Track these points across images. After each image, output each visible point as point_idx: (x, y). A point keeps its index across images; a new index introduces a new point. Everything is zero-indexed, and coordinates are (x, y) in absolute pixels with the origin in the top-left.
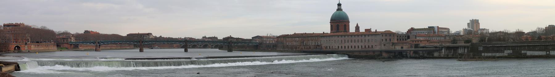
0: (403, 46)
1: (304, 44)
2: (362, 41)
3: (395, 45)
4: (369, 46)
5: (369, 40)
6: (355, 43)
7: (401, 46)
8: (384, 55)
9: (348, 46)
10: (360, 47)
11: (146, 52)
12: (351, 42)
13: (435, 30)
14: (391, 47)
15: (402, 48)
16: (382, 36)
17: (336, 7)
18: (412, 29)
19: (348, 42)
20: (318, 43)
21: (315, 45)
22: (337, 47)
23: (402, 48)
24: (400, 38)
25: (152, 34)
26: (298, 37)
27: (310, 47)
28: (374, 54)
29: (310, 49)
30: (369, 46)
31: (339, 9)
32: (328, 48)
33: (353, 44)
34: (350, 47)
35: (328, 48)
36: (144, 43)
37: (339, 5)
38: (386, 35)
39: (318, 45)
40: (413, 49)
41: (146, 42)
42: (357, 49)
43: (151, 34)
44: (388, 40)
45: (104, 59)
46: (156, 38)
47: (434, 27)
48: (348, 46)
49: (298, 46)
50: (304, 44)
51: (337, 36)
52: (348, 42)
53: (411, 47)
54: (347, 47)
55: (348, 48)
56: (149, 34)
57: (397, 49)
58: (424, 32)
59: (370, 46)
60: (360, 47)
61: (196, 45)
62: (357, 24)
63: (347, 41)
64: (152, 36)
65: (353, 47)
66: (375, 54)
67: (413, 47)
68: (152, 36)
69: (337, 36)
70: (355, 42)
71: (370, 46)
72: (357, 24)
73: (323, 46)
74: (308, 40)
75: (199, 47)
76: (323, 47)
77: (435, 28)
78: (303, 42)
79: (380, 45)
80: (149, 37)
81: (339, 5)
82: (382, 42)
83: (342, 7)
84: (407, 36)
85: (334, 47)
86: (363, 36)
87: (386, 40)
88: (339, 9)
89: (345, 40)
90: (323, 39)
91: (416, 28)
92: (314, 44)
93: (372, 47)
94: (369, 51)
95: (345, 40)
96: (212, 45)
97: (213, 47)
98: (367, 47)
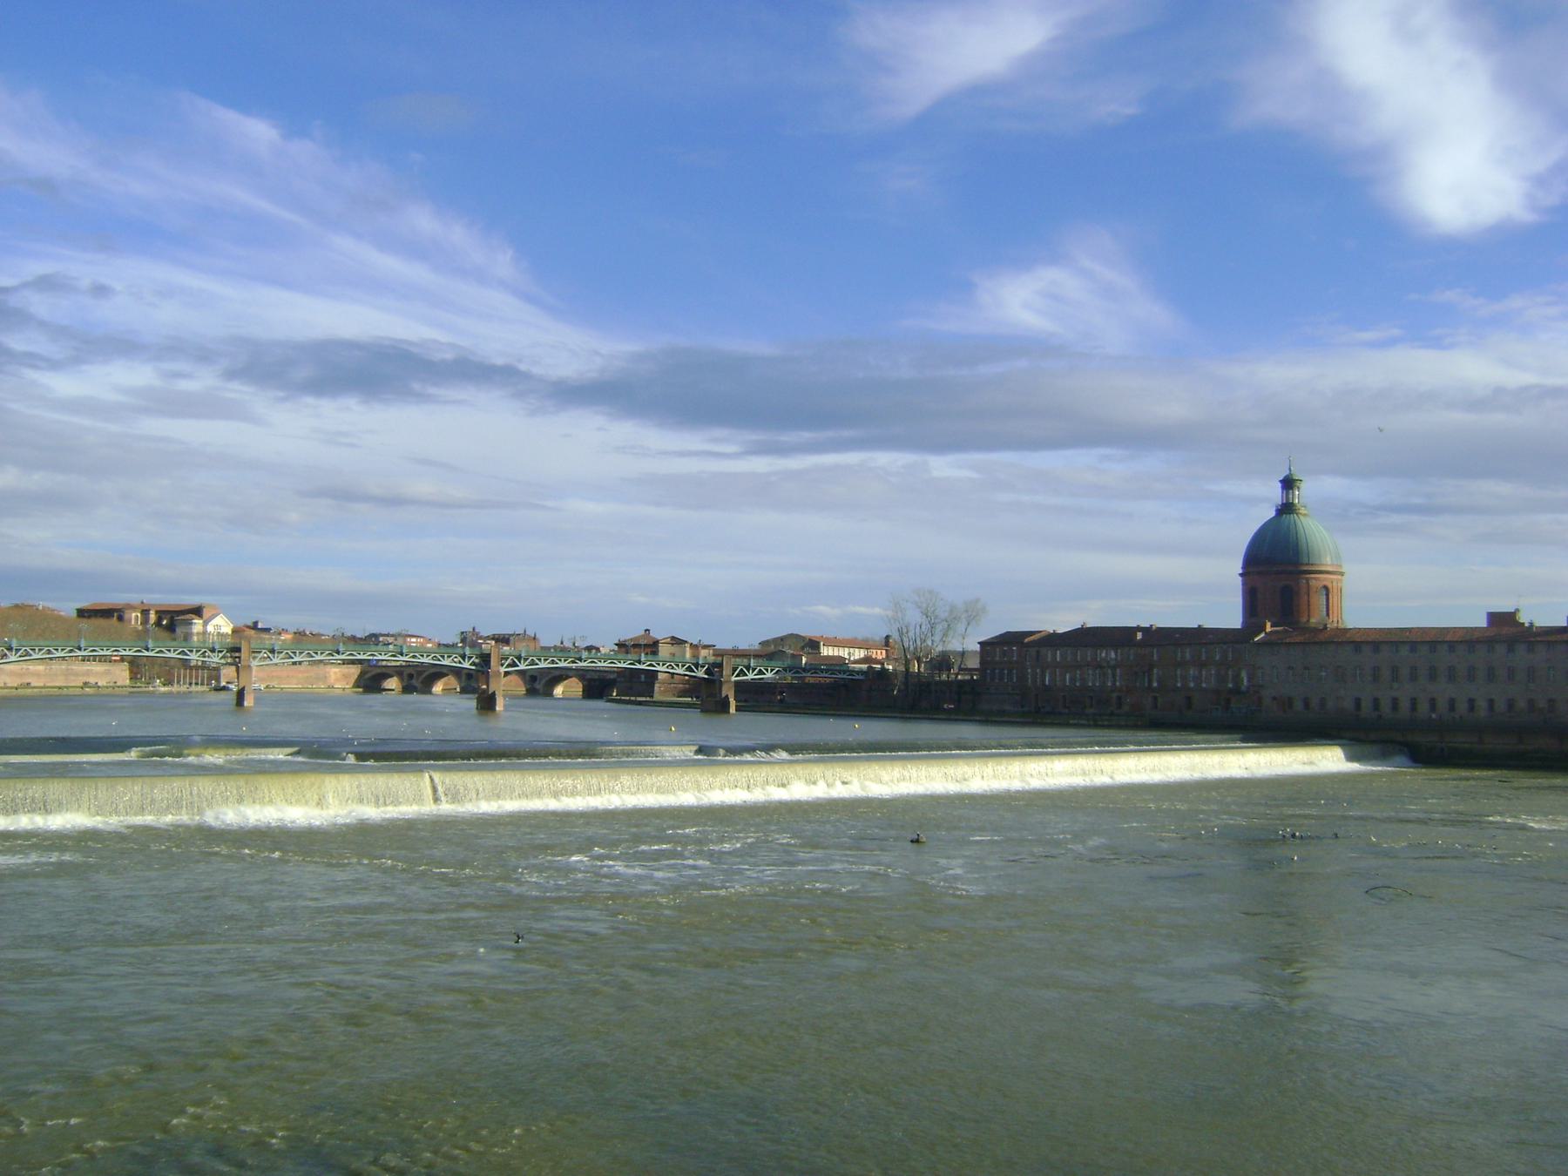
1: (1155, 685)
19: (1413, 677)
20: (1237, 677)
22: (1348, 704)
27: (1189, 698)
32: (1298, 705)
39: (1237, 691)
49: (1112, 691)
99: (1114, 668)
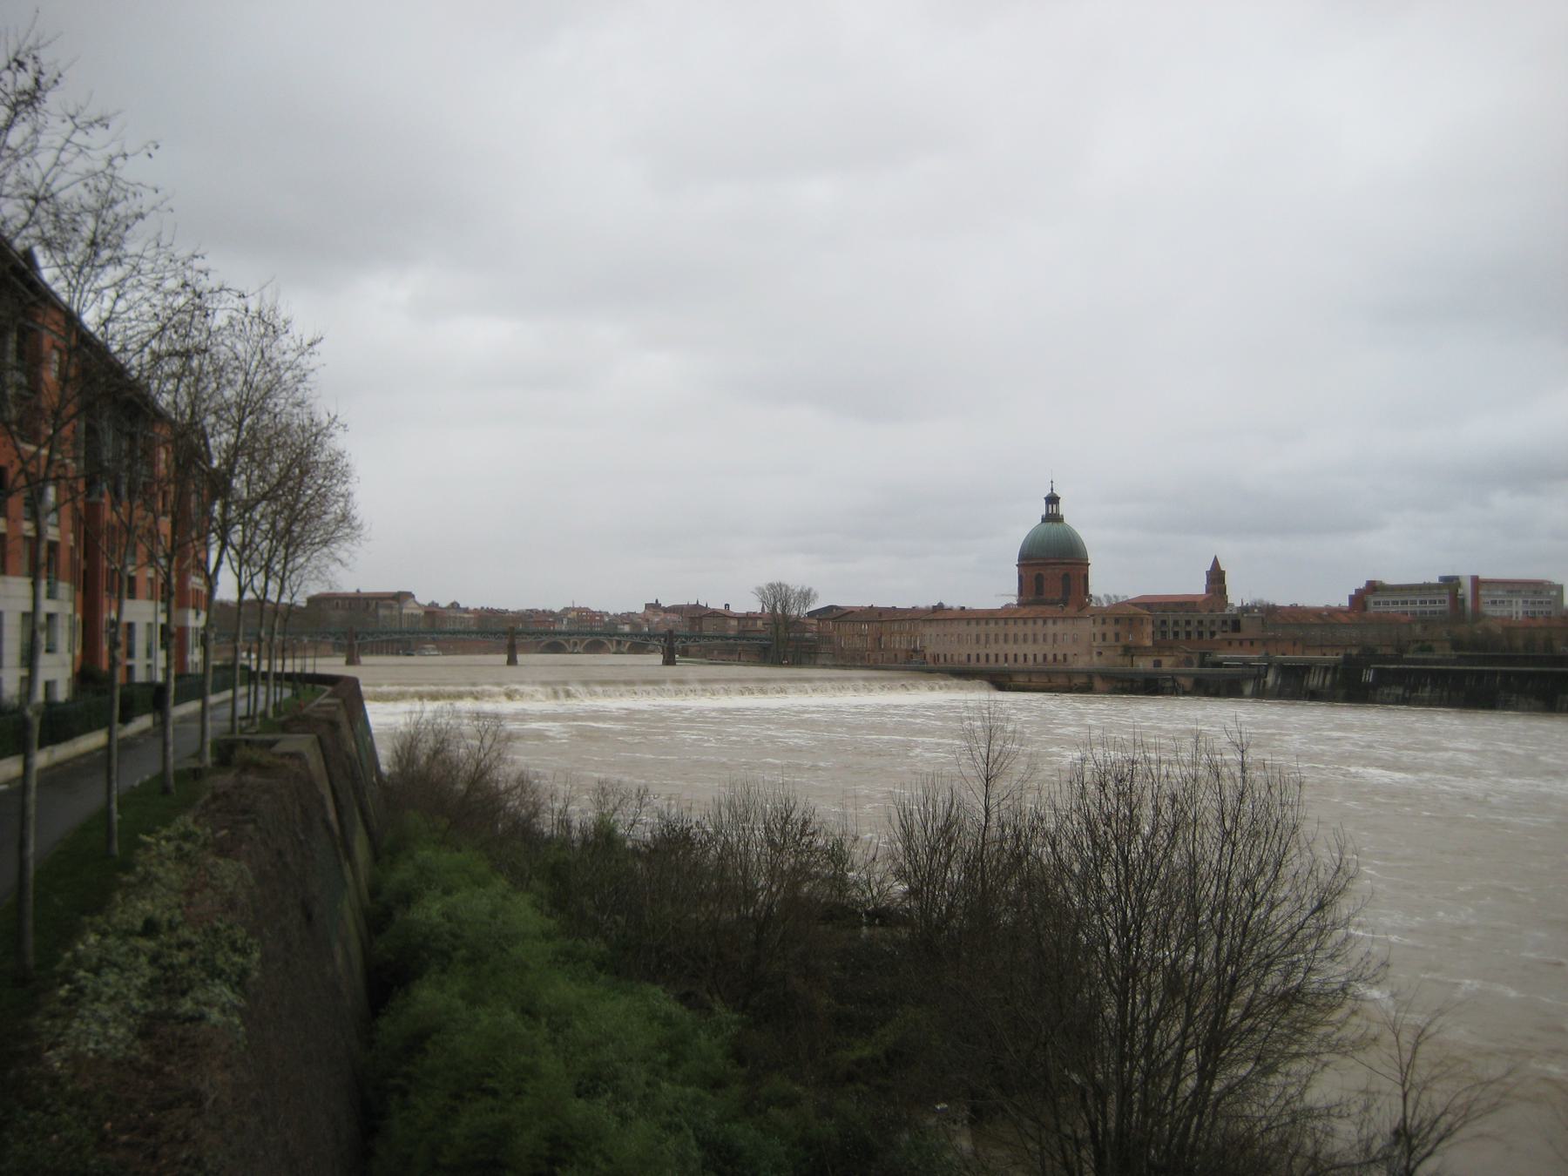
0: (1159, 658)
2: (1035, 641)
3: (1132, 656)
4: (1055, 655)
5: (1055, 635)
6: (1015, 646)
7: (1155, 658)
8: (1098, 683)
9: (1016, 655)
10: (1030, 657)
11: (366, 665)
12: (1006, 641)
13: (1460, 591)
14: (1119, 660)
15: (1158, 664)
16: (1094, 623)
17: (1041, 509)
18: (1373, 587)
19: (996, 641)
21: (907, 651)
22: (964, 658)
23: (1158, 664)
24: (1188, 629)
25: (413, 596)
26: (868, 622)
27: (896, 655)
28: (1070, 681)
29: (896, 661)
30: (1055, 655)
31: (1052, 518)
32: (942, 659)
33: (1011, 649)
34: (1002, 659)
35: (942, 659)
36: (363, 639)
37: (1052, 500)
38: (1104, 622)
39: (915, 651)
40: (1195, 669)
41: (368, 634)
42: (1020, 665)
43: (409, 595)
44: (1110, 636)
45: (628, 663)
46: (432, 612)
47: (1457, 578)
48: (1016, 655)
50: (880, 644)
51: (965, 622)
52: (996, 641)
53: (1189, 663)
54: (992, 658)
55: (987, 660)
56: (401, 597)
57: (1141, 667)
58: (1413, 598)
59: (1060, 657)
60: (1030, 657)
61: (562, 645)
62: (1216, 558)
63: (992, 637)
64: (413, 605)
65: (1011, 658)
66: (1072, 684)
67: (1195, 662)
68: (413, 605)
69: (965, 622)
70: (1035, 641)
71: (1060, 657)
72: (1216, 558)
73: (928, 652)
74: (892, 634)
75: (570, 650)
76: (928, 657)
77: (1462, 580)
78: (880, 639)
79: (1090, 653)
80: (401, 609)
81: (1052, 500)
82: (1095, 644)
83: (1064, 508)
84: (1229, 623)
85: (956, 658)
86: (1001, 623)
87: (1104, 636)
88: (1052, 518)
89: (987, 636)
90: (930, 631)
91: (1390, 580)
92: (904, 646)
93: (1065, 659)
94: (1057, 673)
95: (987, 636)
96: (575, 644)
97: (625, 649)
98: (1050, 657)
99: (867, 636)
